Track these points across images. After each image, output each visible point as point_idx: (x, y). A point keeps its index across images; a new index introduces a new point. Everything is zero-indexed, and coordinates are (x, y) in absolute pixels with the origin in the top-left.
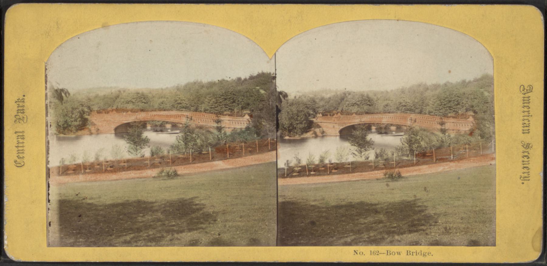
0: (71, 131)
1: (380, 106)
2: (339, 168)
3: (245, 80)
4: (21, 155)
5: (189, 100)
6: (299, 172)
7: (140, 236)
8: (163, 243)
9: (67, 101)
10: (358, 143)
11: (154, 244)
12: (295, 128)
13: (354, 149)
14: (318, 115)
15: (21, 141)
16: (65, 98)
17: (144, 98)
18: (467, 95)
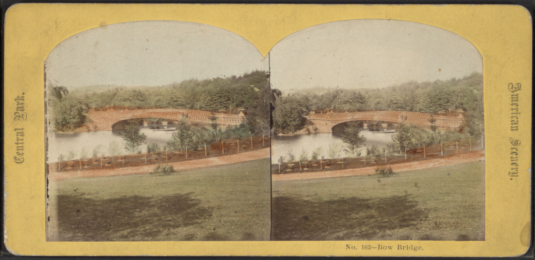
2: (332, 164)
3: (240, 78)
4: (21, 152)
5: (185, 97)
6: (293, 168)
7: (137, 231)
8: (160, 237)
9: (66, 98)
10: (350, 140)
11: (151, 238)
13: (346, 145)
14: (311, 113)
15: (20, 138)
16: (63, 96)
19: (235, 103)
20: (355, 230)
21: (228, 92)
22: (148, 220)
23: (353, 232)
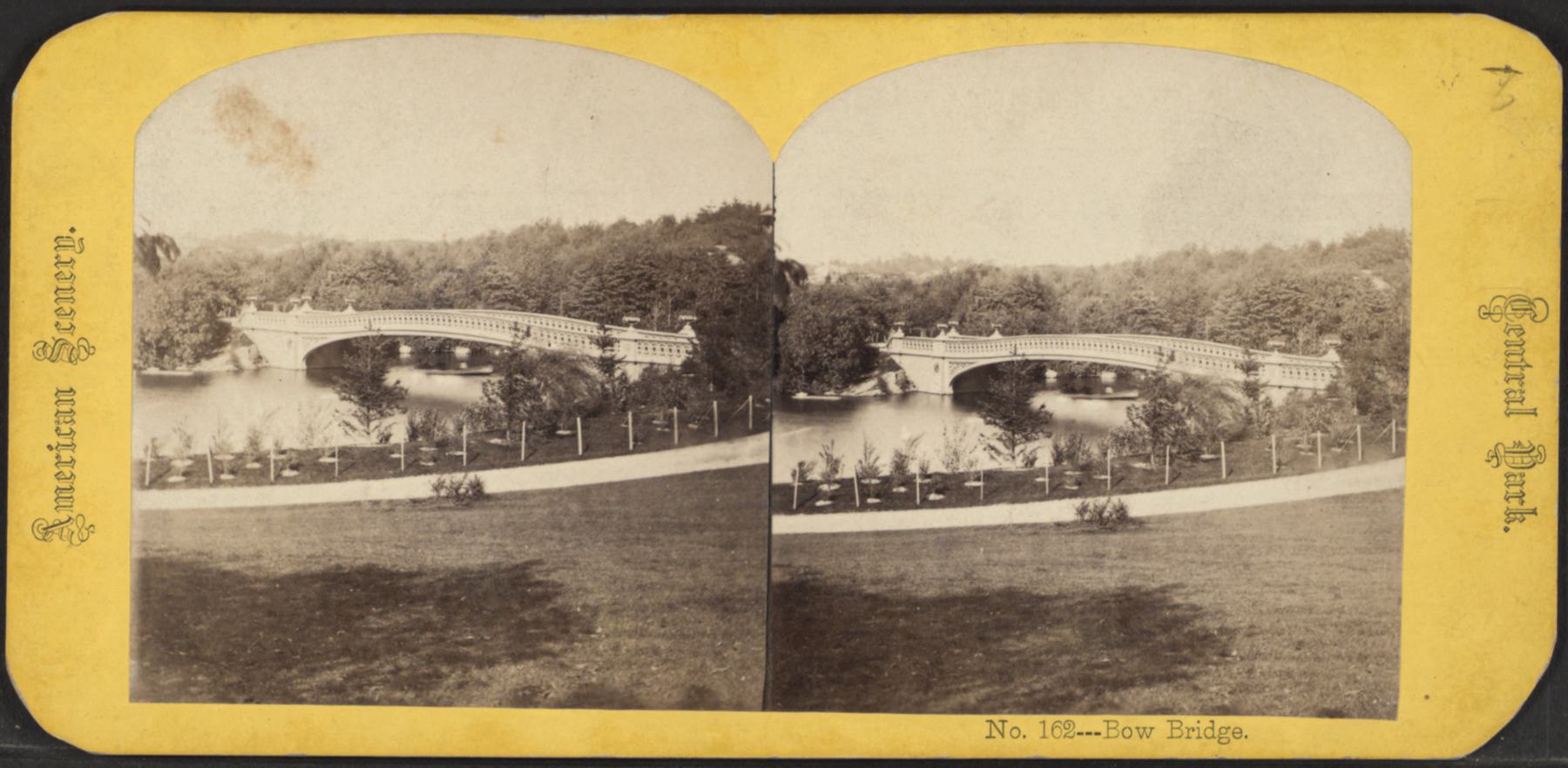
0: (181, 360)
1: (1073, 305)
2: (951, 488)
3: (687, 222)
5: (524, 277)
6: (833, 497)
7: (373, 672)
8: (440, 692)
10: (1004, 417)
11: (411, 695)
12: (826, 370)
13: (349, 408)
14: (893, 334)
16: (164, 263)
17: (394, 270)
18: (1323, 287)
19: (669, 299)
20: (377, 663)
21: (1296, 289)
22: (404, 640)
23: (1006, 694)
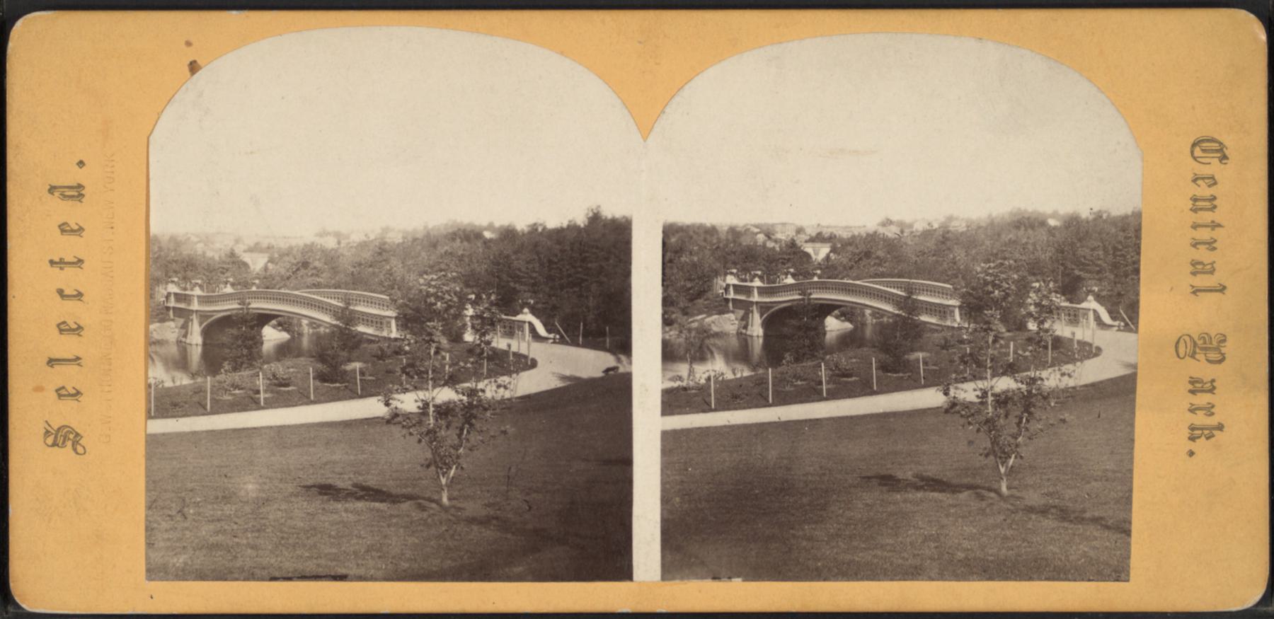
1: (875, 482)
4: (1203, 190)
15: (1203, 254)
